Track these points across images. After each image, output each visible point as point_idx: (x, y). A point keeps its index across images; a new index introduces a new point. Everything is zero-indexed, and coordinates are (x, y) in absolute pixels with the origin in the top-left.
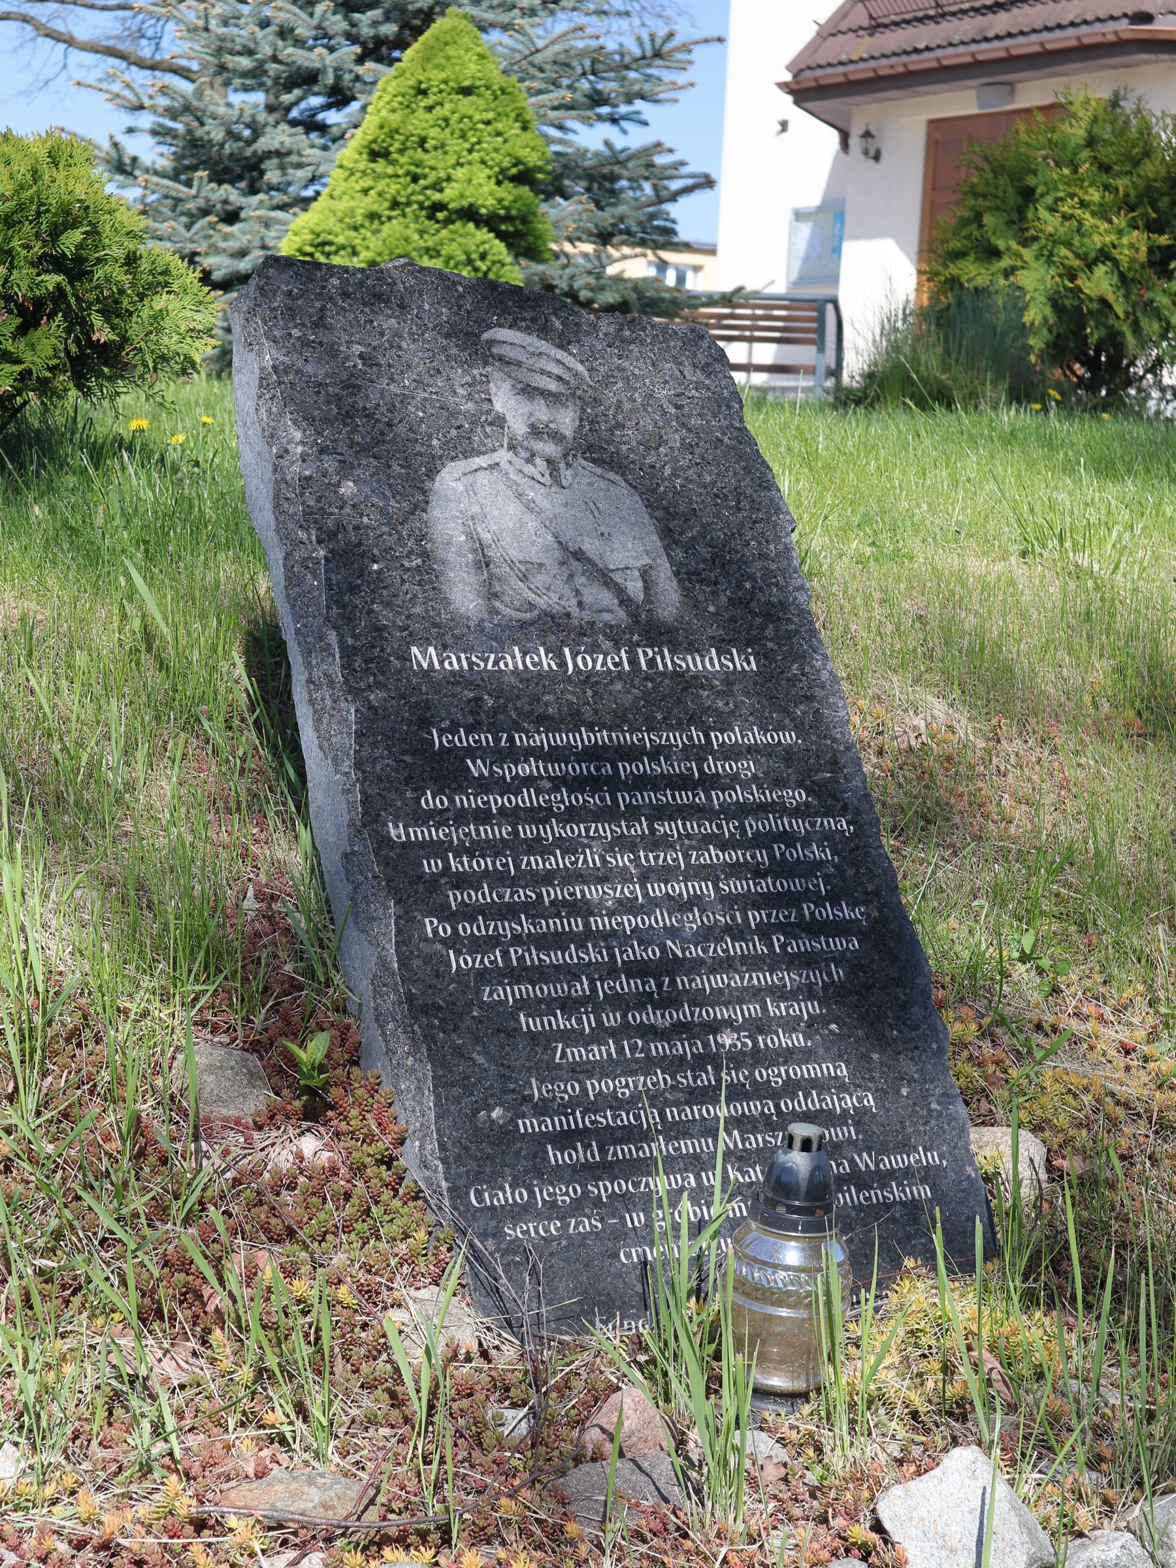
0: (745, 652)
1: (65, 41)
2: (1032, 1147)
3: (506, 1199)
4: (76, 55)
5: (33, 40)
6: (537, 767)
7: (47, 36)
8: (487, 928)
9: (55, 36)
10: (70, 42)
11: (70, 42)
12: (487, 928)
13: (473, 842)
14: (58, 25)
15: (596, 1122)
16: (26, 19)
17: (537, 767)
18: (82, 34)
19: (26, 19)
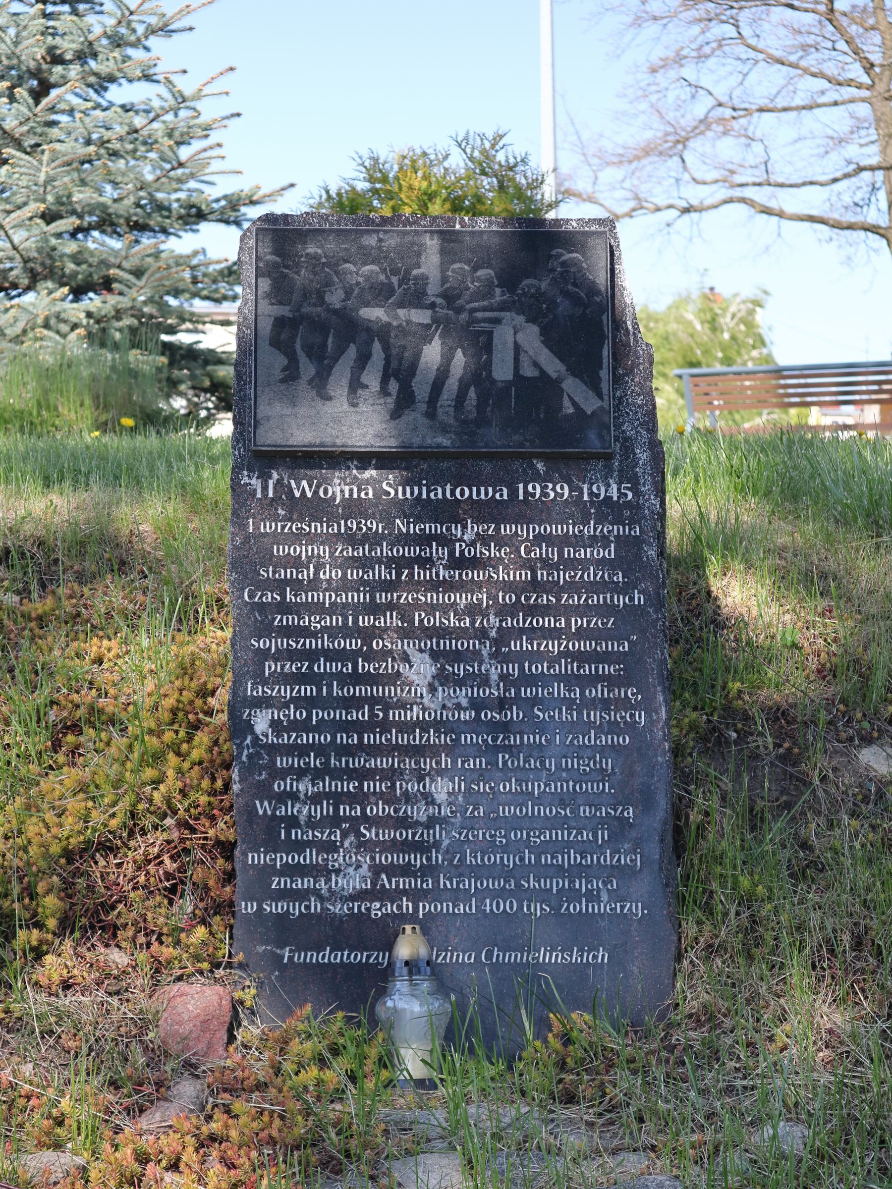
0: (390, 567)
1: (776, 215)
2: (184, 402)
3: (541, 554)
4: (785, 223)
5: (751, 217)
6: (618, 601)
7: (763, 212)
8: (524, 622)
9: (767, 211)
10: (781, 214)
11: (781, 214)
12: (524, 622)
13: (289, 721)
14: (773, 204)
15: (302, 528)
16: (743, 200)
17: (618, 601)
18: (790, 208)
19: (743, 200)
